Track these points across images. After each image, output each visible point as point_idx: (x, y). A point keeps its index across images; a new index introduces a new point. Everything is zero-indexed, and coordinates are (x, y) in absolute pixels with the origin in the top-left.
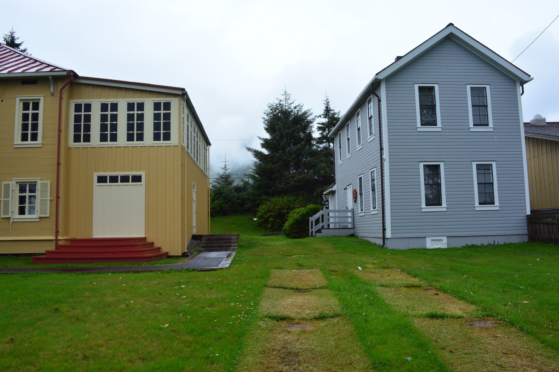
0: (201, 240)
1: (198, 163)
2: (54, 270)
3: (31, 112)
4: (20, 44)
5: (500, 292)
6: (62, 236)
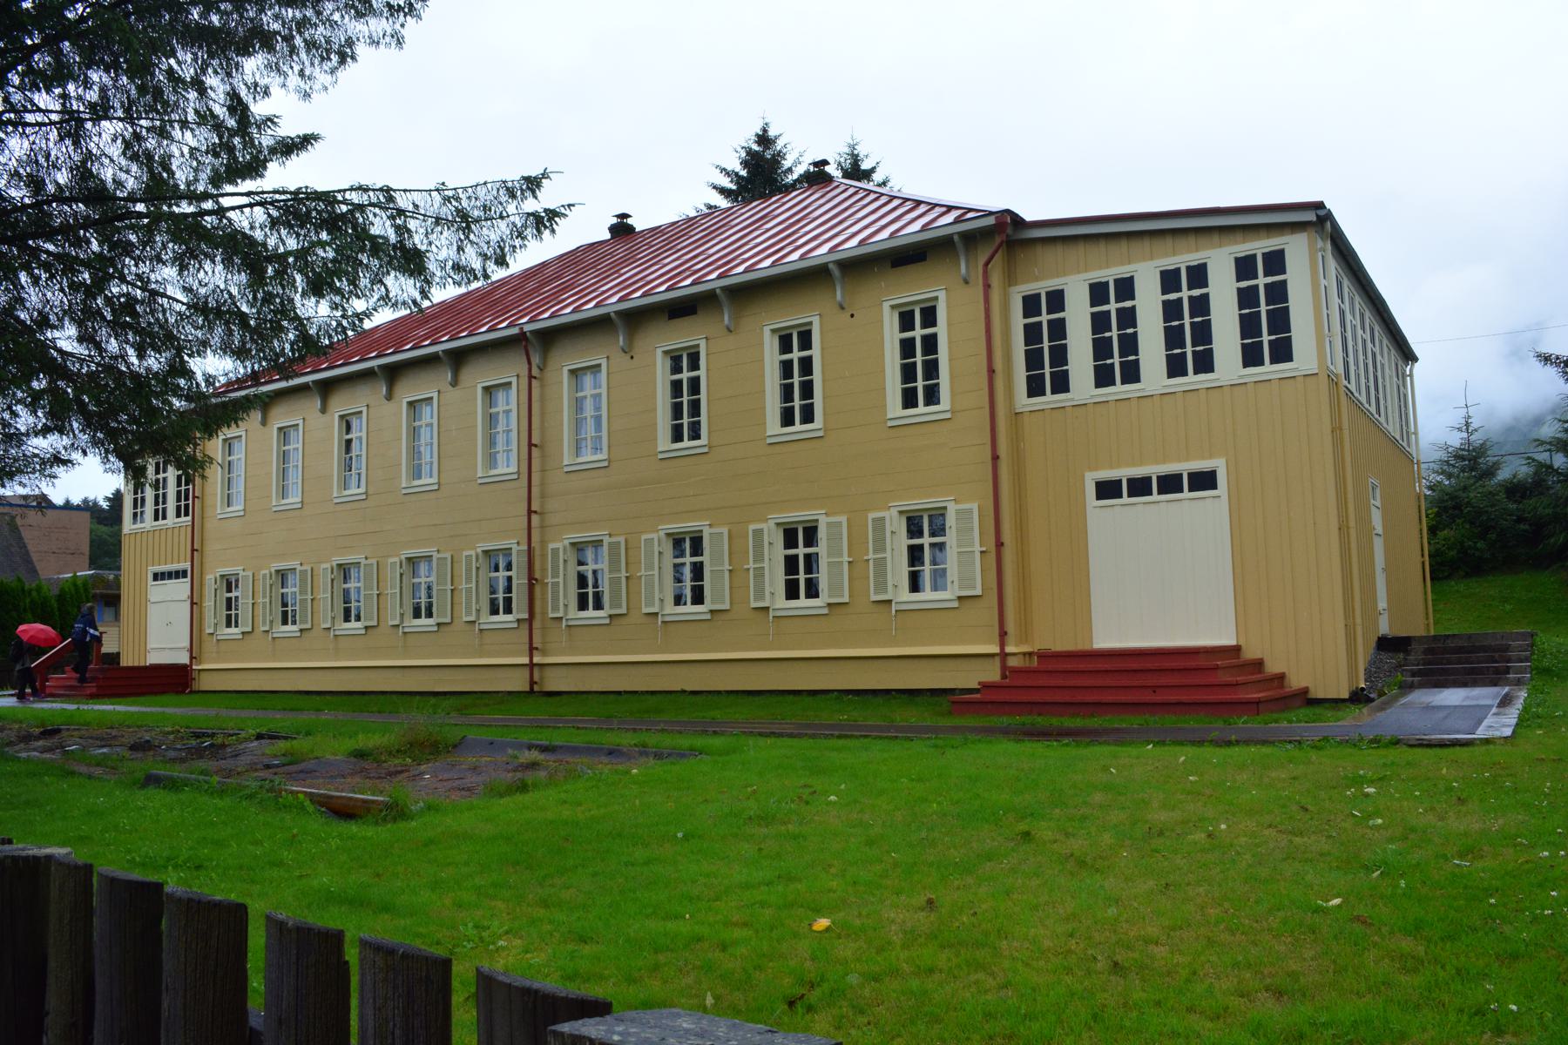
0: (1407, 652)
1: (1382, 419)
2: (1006, 732)
3: (918, 333)
4: (873, 170)
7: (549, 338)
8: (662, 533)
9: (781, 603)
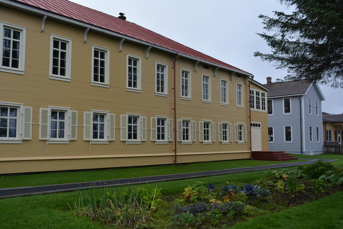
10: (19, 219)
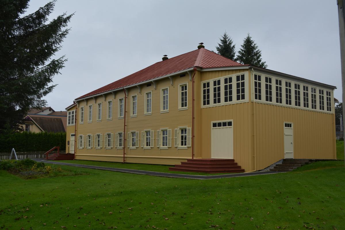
5: (50, 170)
6: (196, 157)
7: (129, 89)
8: (160, 130)
9: (180, 146)
10: (13, 206)
